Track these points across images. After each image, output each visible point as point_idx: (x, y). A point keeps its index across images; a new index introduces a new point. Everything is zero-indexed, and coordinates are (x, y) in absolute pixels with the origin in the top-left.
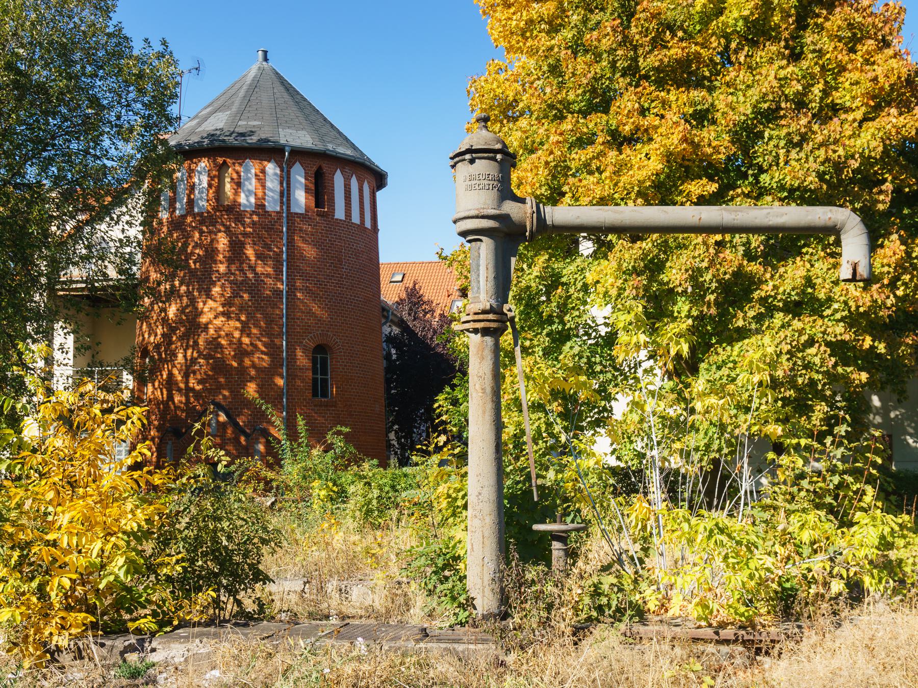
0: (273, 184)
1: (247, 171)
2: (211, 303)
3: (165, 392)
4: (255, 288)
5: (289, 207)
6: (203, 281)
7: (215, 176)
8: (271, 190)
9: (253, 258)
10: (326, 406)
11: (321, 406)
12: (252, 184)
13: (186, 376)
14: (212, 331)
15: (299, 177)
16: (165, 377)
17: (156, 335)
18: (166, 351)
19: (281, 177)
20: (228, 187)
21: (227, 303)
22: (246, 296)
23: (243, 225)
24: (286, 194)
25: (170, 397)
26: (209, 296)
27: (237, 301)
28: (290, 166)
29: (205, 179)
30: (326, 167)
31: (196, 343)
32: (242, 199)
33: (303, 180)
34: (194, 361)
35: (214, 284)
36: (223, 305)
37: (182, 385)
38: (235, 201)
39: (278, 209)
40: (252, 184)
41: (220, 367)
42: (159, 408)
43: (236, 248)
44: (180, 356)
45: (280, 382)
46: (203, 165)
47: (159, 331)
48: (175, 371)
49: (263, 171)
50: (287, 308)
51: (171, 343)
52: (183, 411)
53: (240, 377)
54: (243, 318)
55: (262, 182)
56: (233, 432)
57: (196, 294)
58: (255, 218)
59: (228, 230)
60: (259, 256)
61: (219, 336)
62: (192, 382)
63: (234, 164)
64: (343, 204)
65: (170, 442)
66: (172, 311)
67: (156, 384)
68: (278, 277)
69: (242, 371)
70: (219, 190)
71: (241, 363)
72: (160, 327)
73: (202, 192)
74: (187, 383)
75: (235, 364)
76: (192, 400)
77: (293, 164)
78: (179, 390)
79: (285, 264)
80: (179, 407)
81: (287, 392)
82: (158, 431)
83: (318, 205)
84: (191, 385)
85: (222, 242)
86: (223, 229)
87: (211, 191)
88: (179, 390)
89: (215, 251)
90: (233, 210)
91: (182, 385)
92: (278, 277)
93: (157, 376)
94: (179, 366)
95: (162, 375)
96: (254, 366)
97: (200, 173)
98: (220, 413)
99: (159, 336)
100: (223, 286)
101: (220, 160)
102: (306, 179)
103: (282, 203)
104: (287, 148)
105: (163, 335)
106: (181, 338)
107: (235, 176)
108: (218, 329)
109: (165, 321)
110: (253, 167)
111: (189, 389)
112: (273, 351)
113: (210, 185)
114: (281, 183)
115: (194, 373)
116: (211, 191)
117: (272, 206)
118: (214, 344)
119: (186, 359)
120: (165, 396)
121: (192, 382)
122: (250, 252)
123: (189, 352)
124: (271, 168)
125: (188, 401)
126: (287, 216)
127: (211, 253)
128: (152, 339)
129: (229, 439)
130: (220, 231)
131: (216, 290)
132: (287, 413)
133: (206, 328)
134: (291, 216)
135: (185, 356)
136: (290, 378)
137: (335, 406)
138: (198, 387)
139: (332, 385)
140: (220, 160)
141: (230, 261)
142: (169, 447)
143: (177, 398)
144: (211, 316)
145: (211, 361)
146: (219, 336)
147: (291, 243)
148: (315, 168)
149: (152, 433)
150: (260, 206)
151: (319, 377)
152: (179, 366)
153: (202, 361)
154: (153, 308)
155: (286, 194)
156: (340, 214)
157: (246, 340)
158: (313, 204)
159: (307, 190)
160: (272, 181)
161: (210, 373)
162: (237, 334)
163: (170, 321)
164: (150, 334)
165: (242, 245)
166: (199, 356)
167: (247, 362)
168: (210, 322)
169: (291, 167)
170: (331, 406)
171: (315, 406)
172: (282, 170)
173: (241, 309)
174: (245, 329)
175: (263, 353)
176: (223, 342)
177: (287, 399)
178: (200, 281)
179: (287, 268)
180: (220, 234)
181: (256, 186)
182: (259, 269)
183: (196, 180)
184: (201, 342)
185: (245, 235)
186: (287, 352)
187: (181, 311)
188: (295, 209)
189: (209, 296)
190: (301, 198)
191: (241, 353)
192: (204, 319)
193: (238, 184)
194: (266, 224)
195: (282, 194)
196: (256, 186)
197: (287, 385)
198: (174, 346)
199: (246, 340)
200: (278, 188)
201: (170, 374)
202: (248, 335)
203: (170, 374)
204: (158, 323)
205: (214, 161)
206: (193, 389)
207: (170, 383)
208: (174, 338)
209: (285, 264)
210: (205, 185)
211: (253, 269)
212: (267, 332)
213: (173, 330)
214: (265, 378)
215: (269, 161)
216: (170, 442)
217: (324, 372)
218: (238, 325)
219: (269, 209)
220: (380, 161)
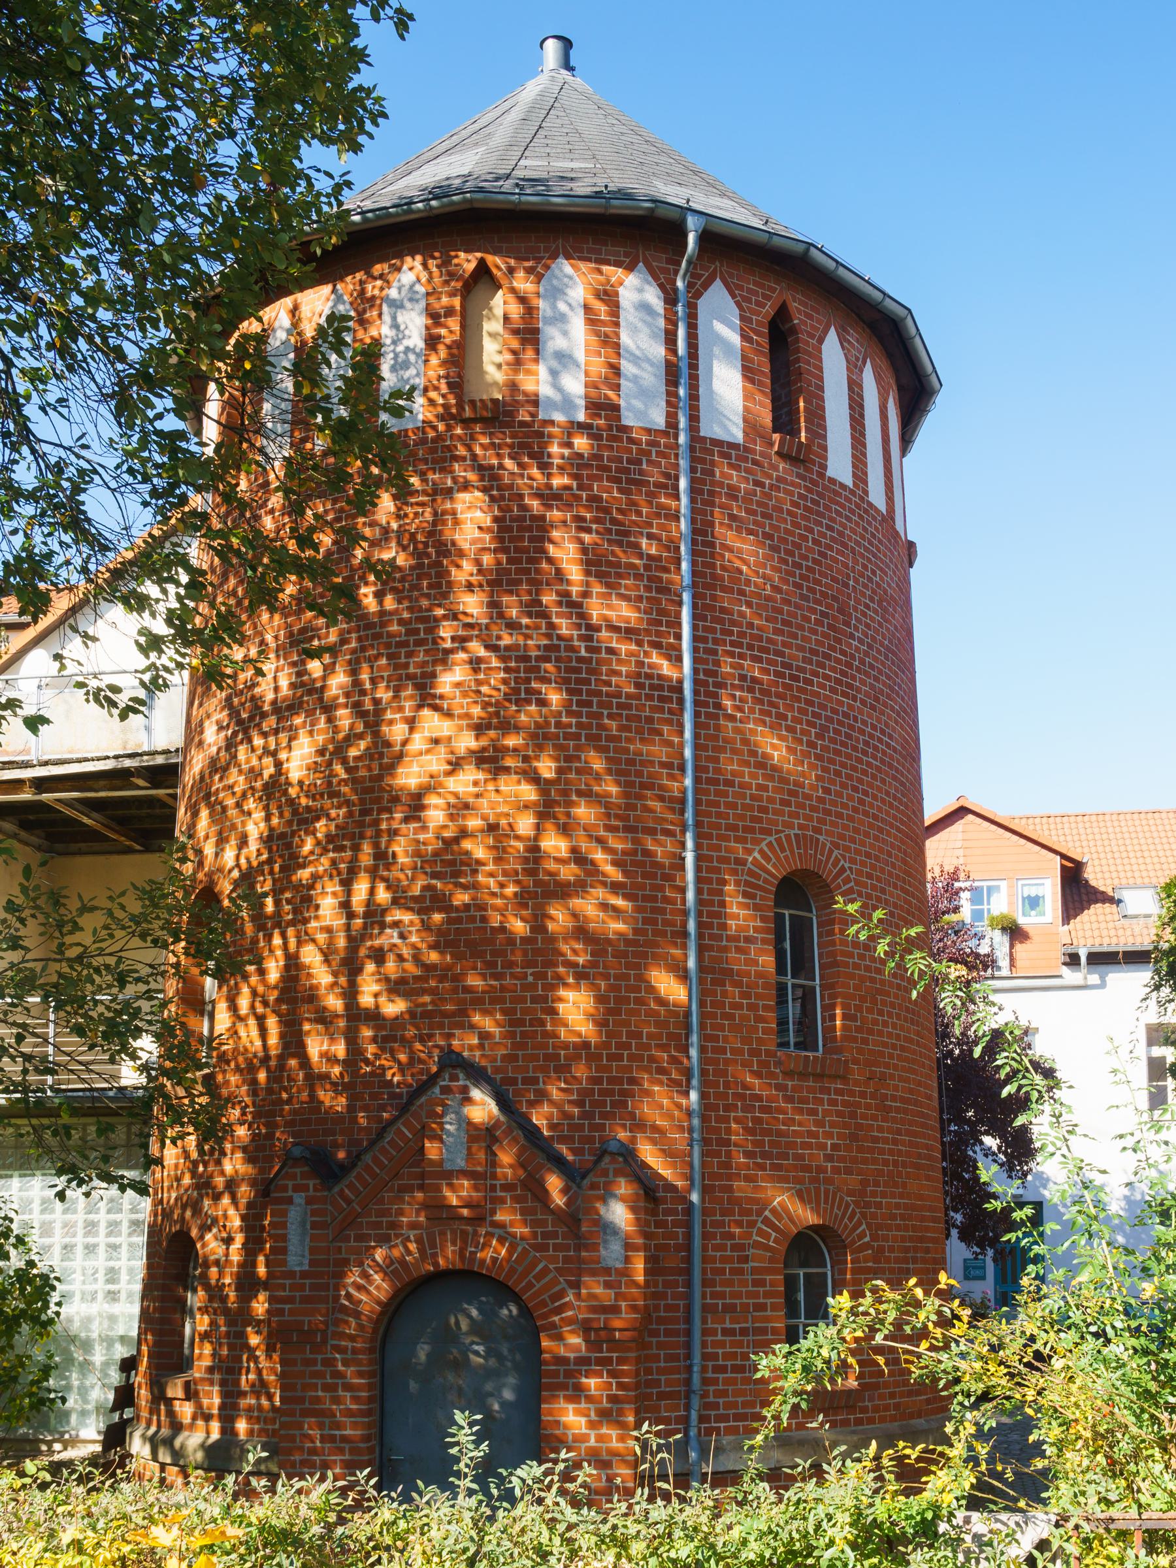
0: (642, 343)
1: (557, 293)
2: (432, 723)
3: (272, 1022)
4: (580, 669)
5: (694, 419)
6: (407, 656)
7: (450, 312)
8: (635, 360)
9: (575, 573)
10: (819, 1077)
11: (803, 1076)
12: (571, 335)
13: (350, 967)
14: (436, 815)
15: (723, 325)
16: (273, 976)
17: (243, 842)
18: (276, 892)
19: (671, 321)
20: (493, 353)
21: (494, 721)
22: (555, 698)
23: (544, 466)
24: (682, 374)
25: (293, 1043)
26: (427, 698)
27: (528, 715)
28: (696, 291)
29: (414, 323)
30: (801, 311)
31: (383, 857)
32: (539, 381)
33: (735, 339)
34: (375, 915)
35: (443, 658)
36: (479, 729)
37: (334, 1003)
38: (513, 386)
39: (658, 419)
40: (571, 335)
41: (466, 935)
42: (254, 1082)
43: (520, 538)
44: (328, 905)
45: (670, 988)
46: (407, 277)
47: (255, 828)
48: (310, 956)
49: (609, 296)
50: (697, 747)
51: (294, 862)
52: (337, 1087)
53: (532, 967)
54: (546, 767)
55: (606, 337)
56: (521, 1164)
57: (384, 695)
58: (581, 443)
59: (490, 480)
60: (594, 563)
61: (464, 833)
62: (369, 991)
63: (511, 271)
64: (848, 451)
65: (299, 1198)
66: (300, 759)
67: (244, 1003)
68: (658, 629)
69: (541, 950)
70: (460, 359)
71: (538, 923)
72: (259, 815)
73: (406, 365)
74: (351, 993)
75: (518, 926)
76: (371, 1050)
77: (706, 285)
78: (324, 1019)
79: (686, 597)
80: (327, 1076)
81: (703, 1016)
82: (250, 1159)
83: (784, 420)
84: (366, 1001)
85: (472, 519)
86: (472, 476)
87: (434, 361)
88: (324, 1019)
89: (447, 551)
90: (509, 421)
91: (334, 1003)
92: (658, 629)
93: (245, 977)
94: (321, 937)
95: (262, 972)
96: (581, 932)
97: (397, 305)
98: (476, 1094)
99: (253, 846)
100: (475, 664)
101: (467, 262)
102: (744, 337)
103: (671, 395)
104: (692, 222)
105: (270, 840)
106: (332, 842)
107: (515, 310)
108: (460, 808)
109: (274, 790)
110: (574, 282)
111: (356, 1015)
112: (647, 881)
113: (432, 342)
114: (670, 340)
115: (379, 956)
116: (434, 361)
117: (644, 410)
118: (448, 861)
119: (351, 915)
120: (273, 1040)
121: (369, 991)
122: (565, 552)
123: (361, 889)
124: (636, 290)
125: (355, 1051)
126: (692, 449)
127: (434, 553)
128: (229, 856)
129: (506, 1187)
130: (466, 487)
131: (450, 680)
132: (703, 1096)
133: (416, 805)
134: (705, 451)
135: (346, 905)
136: (712, 976)
137: (844, 1079)
138: (393, 1008)
139: (829, 1008)
140: (467, 262)
141: (496, 583)
142: (294, 1214)
143: (315, 1047)
144: (436, 763)
145: (437, 917)
146: (464, 833)
147: (701, 531)
148: (769, 309)
149: (228, 1167)
150: (603, 407)
151: (790, 981)
152: (321, 937)
153: (407, 917)
154: (234, 756)
155: (682, 374)
156: (839, 467)
157: (554, 844)
158: (766, 418)
159: (748, 373)
160: (634, 330)
161: (434, 957)
162: (525, 824)
163: (293, 792)
164: (221, 841)
165: (539, 531)
166: (395, 901)
167: (559, 918)
168: (431, 786)
169: (698, 295)
170: (834, 1077)
171: (788, 1074)
172: (671, 299)
173: (540, 737)
174: (550, 808)
175: (615, 888)
176: (480, 853)
177: (702, 1050)
178: (397, 650)
179: (695, 617)
180: (464, 497)
181: (581, 342)
182: (596, 610)
183: (385, 330)
184: (400, 849)
185: (549, 497)
186: (699, 891)
187: (335, 751)
188: (710, 429)
189: (427, 698)
190: (729, 395)
191: (539, 888)
192: (409, 777)
193: (527, 335)
194: (616, 457)
195: (672, 373)
196: (581, 342)
197: (702, 1004)
198: (304, 874)
199: (554, 844)
200: (659, 351)
201: (293, 964)
202: (565, 830)
203: (293, 964)
204: (251, 804)
205: (446, 262)
206: (374, 1016)
207: (294, 996)
208: (308, 846)
209: (686, 597)
210: (416, 340)
211: (574, 607)
212: (627, 819)
213: (304, 819)
214: (617, 971)
215: (630, 268)
216: (299, 1198)
217: (802, 966)
218: (528, 792)
219: (628, 419)
220: (940, 343)
